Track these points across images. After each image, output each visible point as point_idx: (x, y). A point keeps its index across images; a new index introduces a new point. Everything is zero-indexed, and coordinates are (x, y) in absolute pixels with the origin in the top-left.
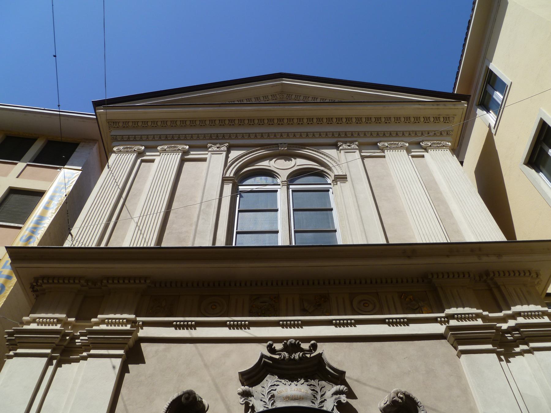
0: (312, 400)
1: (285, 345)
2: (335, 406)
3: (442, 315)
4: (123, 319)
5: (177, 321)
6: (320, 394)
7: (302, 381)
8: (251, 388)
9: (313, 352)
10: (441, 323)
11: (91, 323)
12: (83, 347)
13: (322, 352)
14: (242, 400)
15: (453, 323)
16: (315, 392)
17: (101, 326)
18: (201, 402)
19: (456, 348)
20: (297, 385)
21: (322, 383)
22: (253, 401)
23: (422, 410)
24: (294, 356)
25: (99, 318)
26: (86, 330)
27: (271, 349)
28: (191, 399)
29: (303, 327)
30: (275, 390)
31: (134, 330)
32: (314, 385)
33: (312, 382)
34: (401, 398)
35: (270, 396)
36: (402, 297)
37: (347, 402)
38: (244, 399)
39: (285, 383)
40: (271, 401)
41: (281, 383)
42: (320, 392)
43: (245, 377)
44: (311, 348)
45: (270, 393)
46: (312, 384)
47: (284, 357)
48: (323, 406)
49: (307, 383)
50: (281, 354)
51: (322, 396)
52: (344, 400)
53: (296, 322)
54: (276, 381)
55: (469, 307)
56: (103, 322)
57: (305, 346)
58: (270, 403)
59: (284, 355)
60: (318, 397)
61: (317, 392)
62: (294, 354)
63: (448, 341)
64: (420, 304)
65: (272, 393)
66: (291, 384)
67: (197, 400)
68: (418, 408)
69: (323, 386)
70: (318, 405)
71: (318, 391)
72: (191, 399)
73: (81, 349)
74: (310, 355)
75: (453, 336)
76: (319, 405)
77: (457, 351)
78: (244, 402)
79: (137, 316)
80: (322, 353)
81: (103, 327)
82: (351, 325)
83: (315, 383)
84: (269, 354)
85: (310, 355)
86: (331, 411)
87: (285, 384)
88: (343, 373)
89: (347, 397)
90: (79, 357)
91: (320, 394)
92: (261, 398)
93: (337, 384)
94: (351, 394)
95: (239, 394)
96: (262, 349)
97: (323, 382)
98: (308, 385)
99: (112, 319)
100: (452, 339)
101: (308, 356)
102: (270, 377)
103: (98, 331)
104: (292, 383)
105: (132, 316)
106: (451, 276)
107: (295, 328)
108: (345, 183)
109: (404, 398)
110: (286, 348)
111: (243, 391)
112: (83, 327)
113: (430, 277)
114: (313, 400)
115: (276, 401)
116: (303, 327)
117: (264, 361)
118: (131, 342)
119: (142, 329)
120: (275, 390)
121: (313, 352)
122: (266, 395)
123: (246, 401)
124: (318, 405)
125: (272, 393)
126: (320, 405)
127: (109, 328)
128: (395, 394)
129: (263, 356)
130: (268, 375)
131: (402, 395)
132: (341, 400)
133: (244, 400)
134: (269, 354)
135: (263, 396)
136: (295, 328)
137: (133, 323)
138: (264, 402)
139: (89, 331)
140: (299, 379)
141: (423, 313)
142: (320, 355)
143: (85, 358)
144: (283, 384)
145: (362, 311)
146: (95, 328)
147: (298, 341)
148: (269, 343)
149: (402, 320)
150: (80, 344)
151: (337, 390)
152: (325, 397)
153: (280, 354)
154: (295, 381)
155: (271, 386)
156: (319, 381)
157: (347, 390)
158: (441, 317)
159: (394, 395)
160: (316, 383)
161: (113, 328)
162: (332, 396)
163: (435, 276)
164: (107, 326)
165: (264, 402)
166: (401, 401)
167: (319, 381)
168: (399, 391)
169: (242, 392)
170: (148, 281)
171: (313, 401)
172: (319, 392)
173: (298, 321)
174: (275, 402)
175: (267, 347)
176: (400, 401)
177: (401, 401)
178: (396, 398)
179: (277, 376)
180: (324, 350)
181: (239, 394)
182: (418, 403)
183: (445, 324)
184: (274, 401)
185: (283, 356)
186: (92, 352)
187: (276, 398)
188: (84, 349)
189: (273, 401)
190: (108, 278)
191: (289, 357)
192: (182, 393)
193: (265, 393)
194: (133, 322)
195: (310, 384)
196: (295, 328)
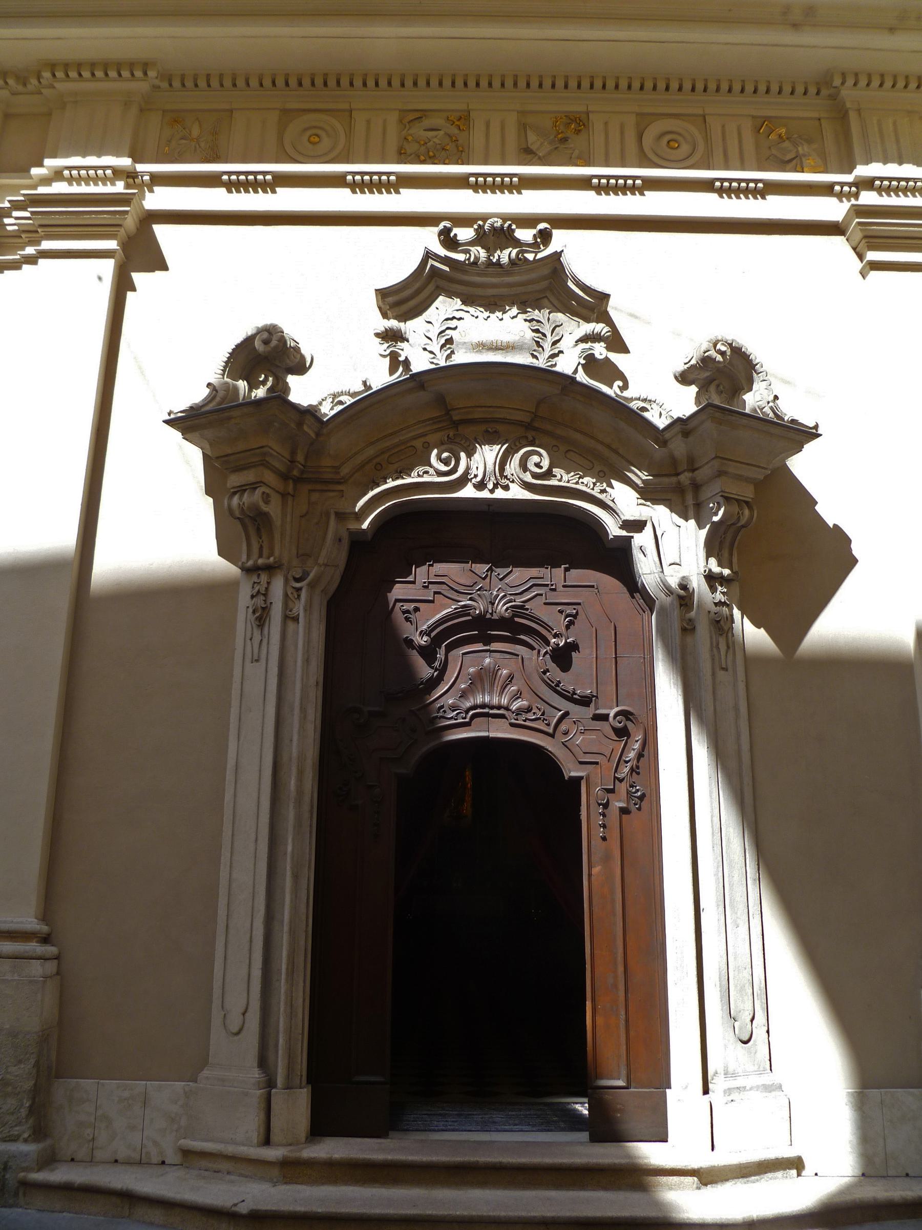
0: (533, 352)
1: (480, 231)
2: (580, 366)
3: (849, 178)
4: (104, 168)
5: (230, 173)
6: (550, 339)
7: (515, 311)
8: (402, 325)
9: (542, 248)
10: (840, 196)
11: (31, 180)
12: (23, 236)
13: (561, 250)
14: (384, 348)
15: (868, 198)
16: (540, 335)
17: (54, 184)
18: (297, 350)
19: (861, 257)
20: (502, 319)
21: (557, 317)
22: (406, 351)
23: (761, 379)
24: (499, 256)
25: (48, 168)
26: (24, 195)
27: (449, 241)
28: (274, 343)
29: (522, 191)
30: (455, 328)
31: (134, 194)
32: (538, 321)
33: (536, 314)
34: (723, 353)
35: (443, 341)
36: (761, 131)
37: (607, 359)
38: (386, 345)
39: (476, 316)
40: (446, 351)
41: (468, 313)
42: (551, 335)
43: (391, 299)
44: (539, 240)
45: (443, 334)
46: (536, 318)
47: (477, 258)
48: (556, 363)
49: (524, 316)
50: (471, 250)
51: (555, 343)
52: (601, 354)
53: (507, 179)
54: (457, 310)
55: (914, 164)
56: (58, 175)
57: (525, 235)
58: (442, 356)
59: (476, 253)
60: (547, 345)
61: (544, 335)
62: (498, 252)
63: (847, 240)
64: (800, 149)
65: (449, 335)
66: (489, 317)
67: (288, 346)
68: (755, 375)
69: (558, 324)
70: (544, 363)
71: (547, 333)
72: (274, 343)
73: (20, 240)
74: (536, 256)
75: (860, 229)
76: (547, 362)
77: (862, 262)
78: (388, 352)
79: (136, 161)
80: (563, 251)
81: (60, 188)
82: (633, 189)
83: (542, 316)
84: (442, 252)
85: (536, 256)
86: (572, 374)
87: (477, 317)
88: (604, 297)
89: (609, 348)
90: (18, 257)
91: (550, 339)
92: (425, 345)
93: (588, 320)
94: (617, 343)
95: (377, 335)
96: (429, 238)
97: (560, 315)
98: (526, 320)
99: (78, 168)
100: (859, 235)
101: (530, 257)
102: (444, 302)
103: (50, 197)
104: (491, 315)
105: (125, 162)
106: (888, 83)
107: (503, 192)
108: (582, 349)
109: (729, 353)
110: (481, 239)
111: (386, 329)
112: (15, 189)
113: (837, 82)
114: (534, 350)
115: (456, 352)
116: (522, 191)
117: (432, 265)
118: (130, 223)
119: (151, 191)
120: (455, 328)
121: (542, 248)
122: (434, 338)
123: (391, 349)
124: (545, 361)
125: (449, 335)
126: (550, 361)
127: (75, 189)
128: (712, 345)
129: (428, 255)
130: (441, 298)
131: (726, 346)
132: (593, 354)
133: (388, 347)
134: (442, 252)
135: (429, 341)
136: (504, 193)
137: (128, 177)
138: (431, 352)
139: (30, 197)
140: (507, 308)
141: (803, 172)
142: (557, 255)
143: (32, 260)
144: (473, 316)
145: (664, 159)
146: (42, 190)
147: (510, 222)
148: (444, 226)
149: (752, 185)
150: (16, 228)
151: (588, 332)
152: (561, 346)
153: (467, 252)
154: (499, 312)
155: (447, 319)
156: (549, 313)
157: (609, 334)
158: (842, 184)
159: (707, 346)
160: (543, 316)
161: (83, 189)
162: (576, 345)
163: (850, 82)
164: (70, 184)
165: (431, 352)
166: (721, 360)
167: (549, 313)
168: (720, 338)
169: (383, 332)
170: (152, 74)
171: (535, 353)
172: (548, 334)
173: (511, 176)
174: (454, 354)
175: (439, 235)
176: (719, 358)
177: (721, 360)
178: (712, 353)
179: (458, 300)
180: (565, 246)
181: (377, 335)
182: (757, 364)
183: (849, 201)
184: (451, 351)
185: (475, 255)
186: (47, 245)
187: (457, 345)
188: (27, 239)
189: (449, 351)
190: (53, 67)
191: (488, 258)
192: (254, 332)
193: (434, 332)
194: (130, 176)
195: (531, 318)
196: (503, 193)
